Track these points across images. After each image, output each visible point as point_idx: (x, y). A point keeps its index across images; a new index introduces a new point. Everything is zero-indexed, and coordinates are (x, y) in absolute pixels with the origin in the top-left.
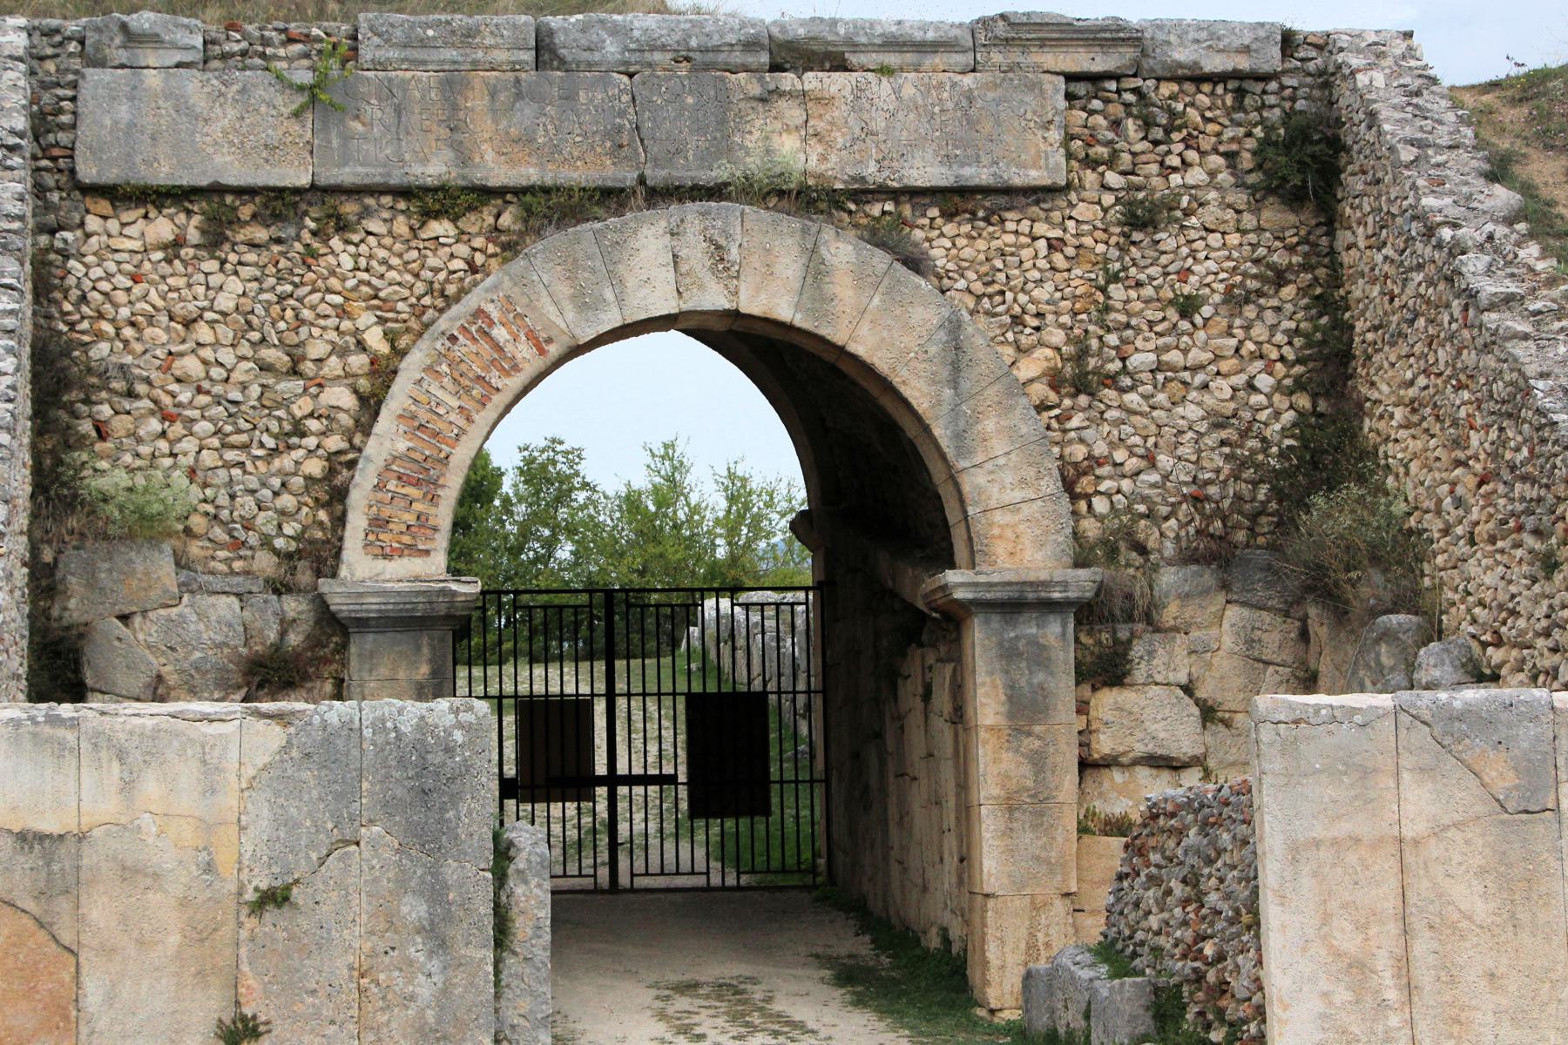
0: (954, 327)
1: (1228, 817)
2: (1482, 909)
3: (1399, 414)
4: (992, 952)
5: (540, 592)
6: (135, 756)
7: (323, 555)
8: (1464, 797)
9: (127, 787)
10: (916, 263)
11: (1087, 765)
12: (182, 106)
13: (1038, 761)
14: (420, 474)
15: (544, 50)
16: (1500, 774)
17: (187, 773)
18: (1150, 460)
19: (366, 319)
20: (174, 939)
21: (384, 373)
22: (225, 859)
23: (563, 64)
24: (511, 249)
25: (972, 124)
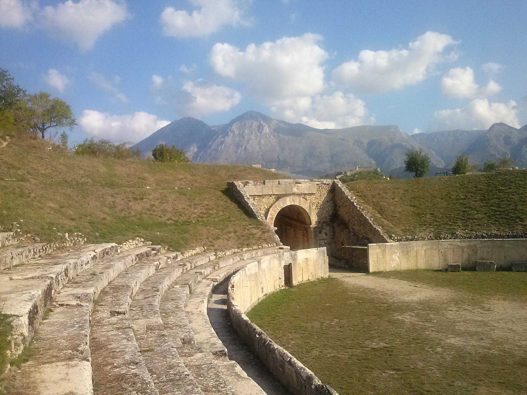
15: (279, 183)
16: (382, 248)
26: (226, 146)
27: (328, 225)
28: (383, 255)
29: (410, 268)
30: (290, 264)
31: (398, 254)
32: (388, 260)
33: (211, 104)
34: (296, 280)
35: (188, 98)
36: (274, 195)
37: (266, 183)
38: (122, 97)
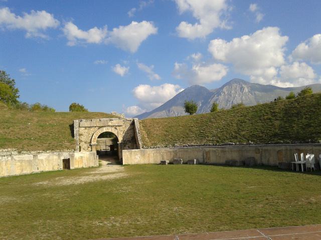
7: (91, 142)
10: (116, 129)
26: (219, 101)
27: (130, 142)
28: (131, 156)
30: (69, 159)
32: (133, 158)
33: (210, 76)
34: (73, 166)
35: (194, 74)
38: (157, 76)
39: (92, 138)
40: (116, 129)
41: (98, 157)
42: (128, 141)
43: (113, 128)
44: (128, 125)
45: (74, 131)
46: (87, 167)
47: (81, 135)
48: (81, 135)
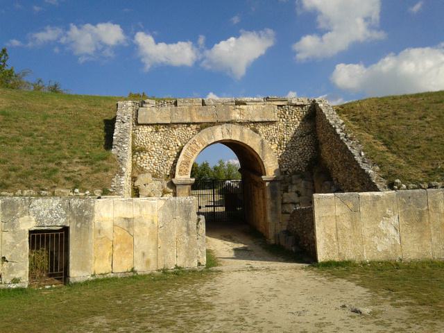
0: (262, 141)
1: (310, 213)
2: (349, 226)
3: (327, 153)
4: (270, 231)
5: (257, 102)
6: (141, 206)
7: (173, 175)
8: (345, 209)
9: (141, 210)
10: (256, 132)
11: (283, 204)
12: (153, 112)
13: (276, 203)
14: (187, 163)
15: (203, 103)
16: (351, 206)
17: (150, 208)
18: (291, 160)
19: (178, 141)
20: (148, 234)
21: (181, 149)
22: (156, 222)
23: (206, 105)
24: (199, 131)
25: (264, 112)
27: (302, 177)
28: (354, 222)
29: (430, 256)
30: (66, 229)
31: (394, 220)
36: (194, 123)
37: (178, 104)
39: (175, 162)
40: (256, 132)
41: (203, 226)
42: (295, 173)
43: (246, 130)
44: (295, 122)
45: (113, 128)
46: (153, 268)
47: (142, 150)
48: (142, 150)
